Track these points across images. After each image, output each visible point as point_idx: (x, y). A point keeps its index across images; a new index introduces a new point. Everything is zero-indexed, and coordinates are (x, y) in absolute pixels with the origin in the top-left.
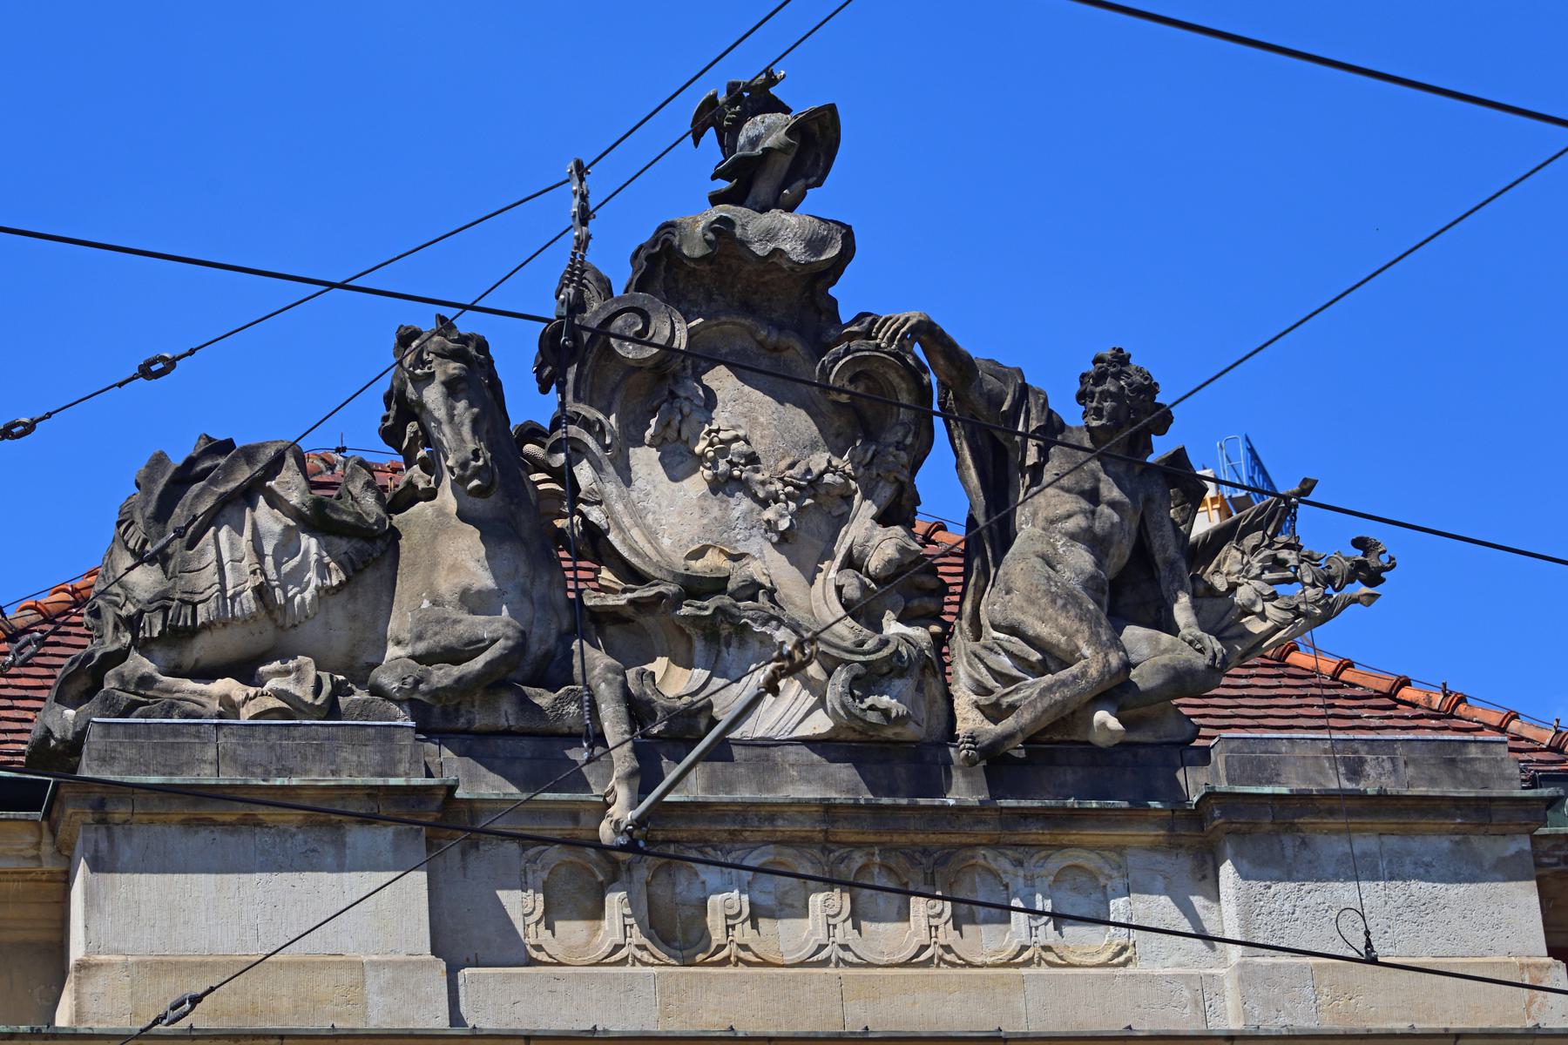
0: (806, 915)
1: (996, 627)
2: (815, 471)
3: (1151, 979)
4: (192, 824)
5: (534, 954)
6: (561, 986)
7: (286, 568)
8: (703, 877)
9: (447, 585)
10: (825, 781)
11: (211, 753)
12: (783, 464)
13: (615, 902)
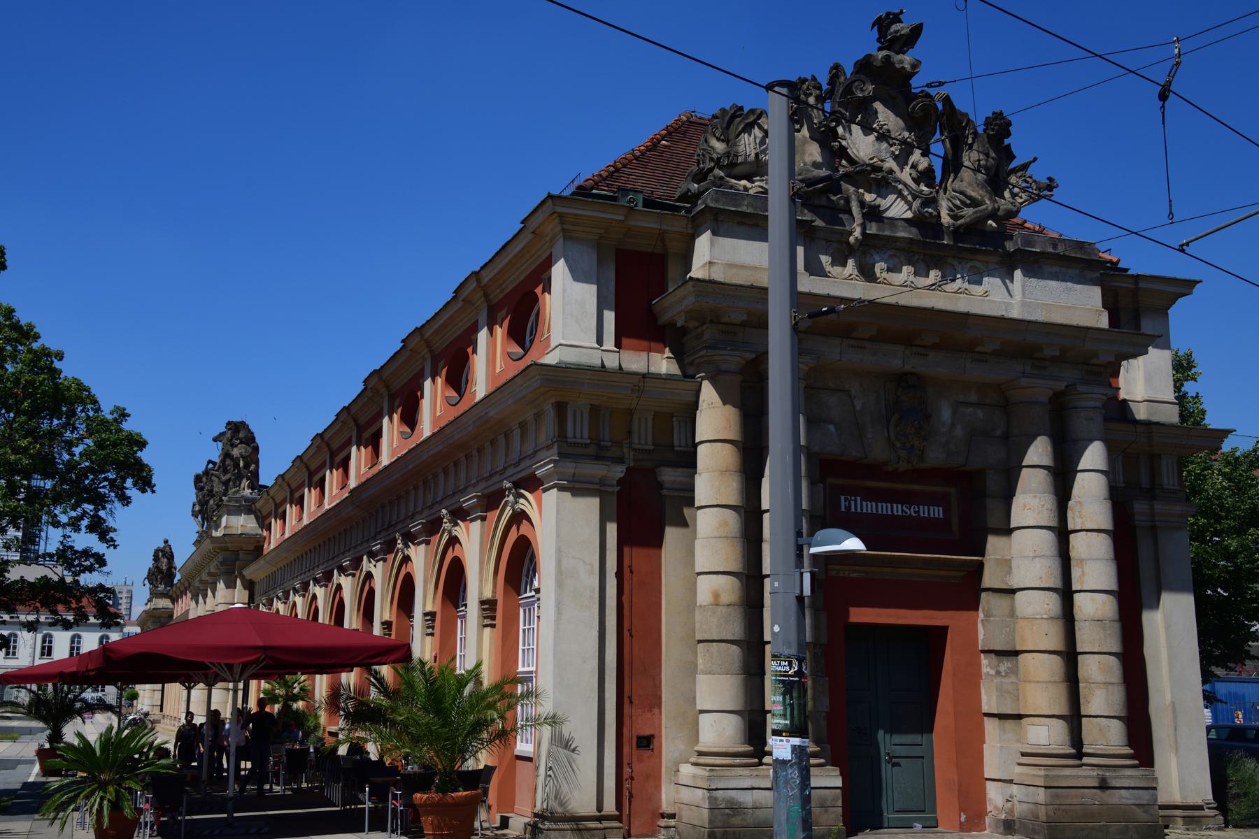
0: (901, 272)
1: (954, 191)
2: (906, 137)
3: (994, 302)
4: (740, 224)
5: (828, 274)
6: (836, 285)
7: (762, 148)
8: (874, 257)
9: (808, 159)
10: (909, 232)
11: (746, 203)
12: (897, 134)
13: (851, 262)
